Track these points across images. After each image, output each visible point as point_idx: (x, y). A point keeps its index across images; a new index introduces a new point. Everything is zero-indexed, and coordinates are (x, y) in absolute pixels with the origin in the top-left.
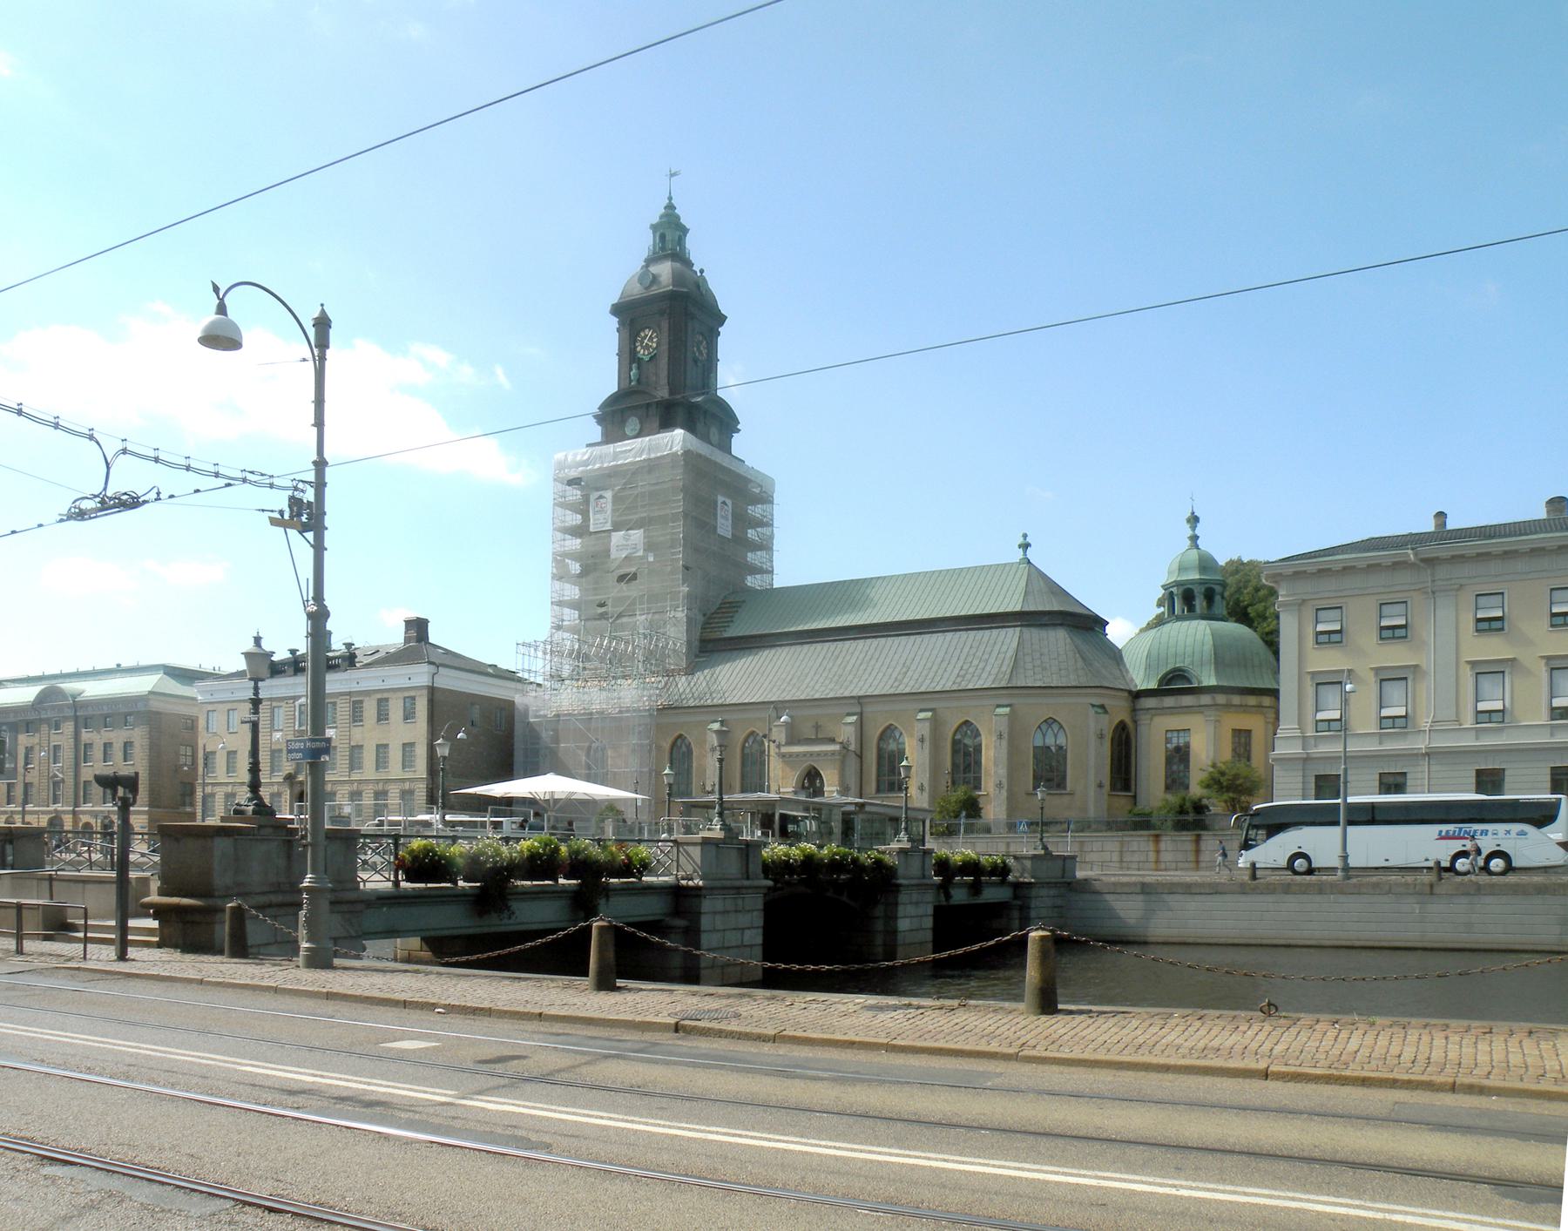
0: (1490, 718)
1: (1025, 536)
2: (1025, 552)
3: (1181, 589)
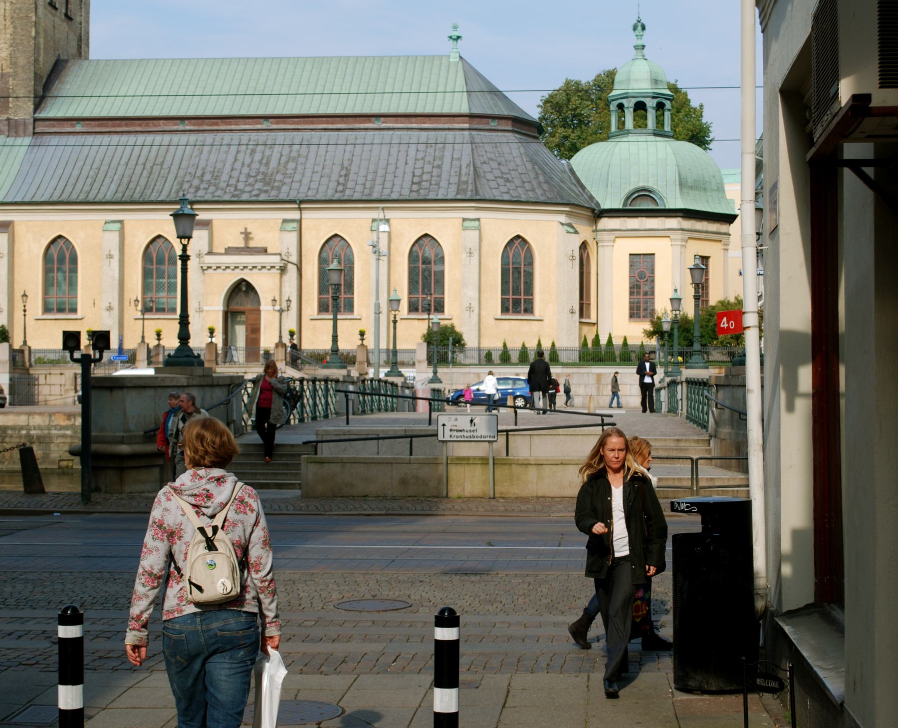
3: (634, 101)
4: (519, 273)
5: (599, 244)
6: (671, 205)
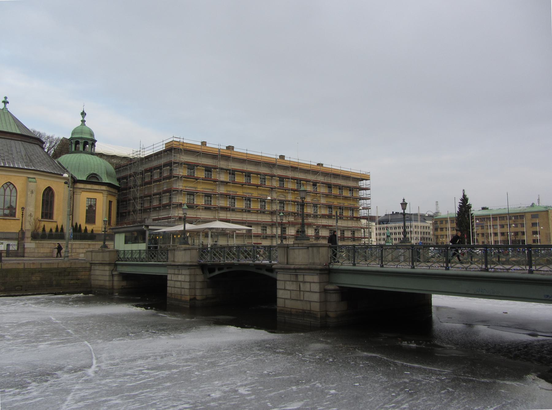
0: (10, 185)
1: (6, 98)
2: (5, 106)
3: (84, 141)
4: (48, 202)
5: (75, 193)
6: (104, 181)
